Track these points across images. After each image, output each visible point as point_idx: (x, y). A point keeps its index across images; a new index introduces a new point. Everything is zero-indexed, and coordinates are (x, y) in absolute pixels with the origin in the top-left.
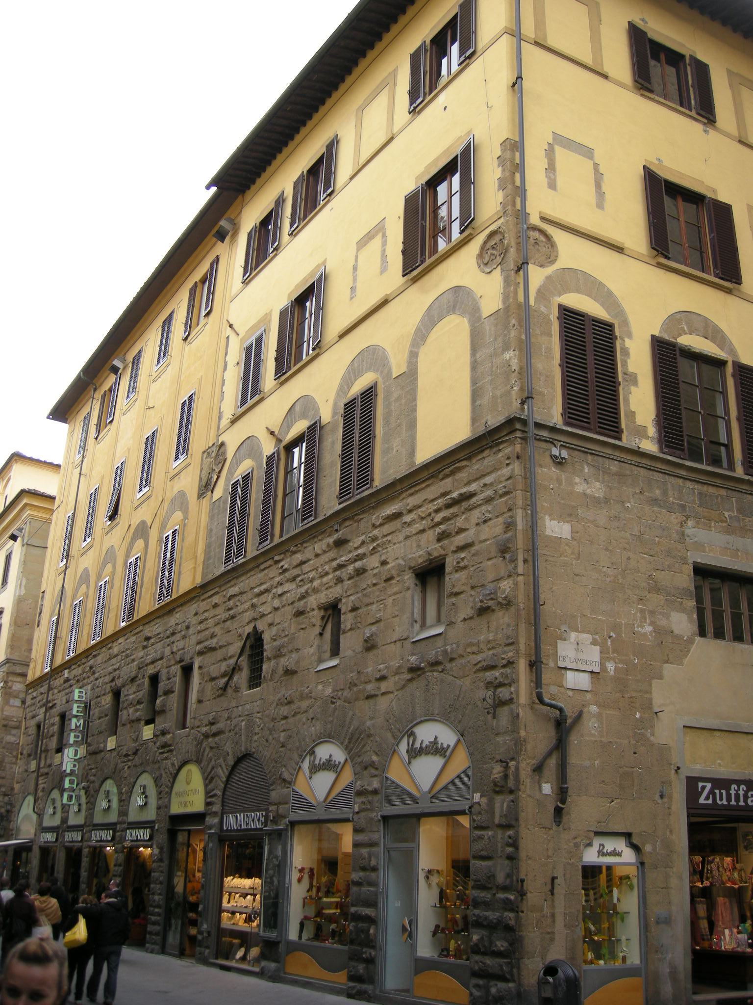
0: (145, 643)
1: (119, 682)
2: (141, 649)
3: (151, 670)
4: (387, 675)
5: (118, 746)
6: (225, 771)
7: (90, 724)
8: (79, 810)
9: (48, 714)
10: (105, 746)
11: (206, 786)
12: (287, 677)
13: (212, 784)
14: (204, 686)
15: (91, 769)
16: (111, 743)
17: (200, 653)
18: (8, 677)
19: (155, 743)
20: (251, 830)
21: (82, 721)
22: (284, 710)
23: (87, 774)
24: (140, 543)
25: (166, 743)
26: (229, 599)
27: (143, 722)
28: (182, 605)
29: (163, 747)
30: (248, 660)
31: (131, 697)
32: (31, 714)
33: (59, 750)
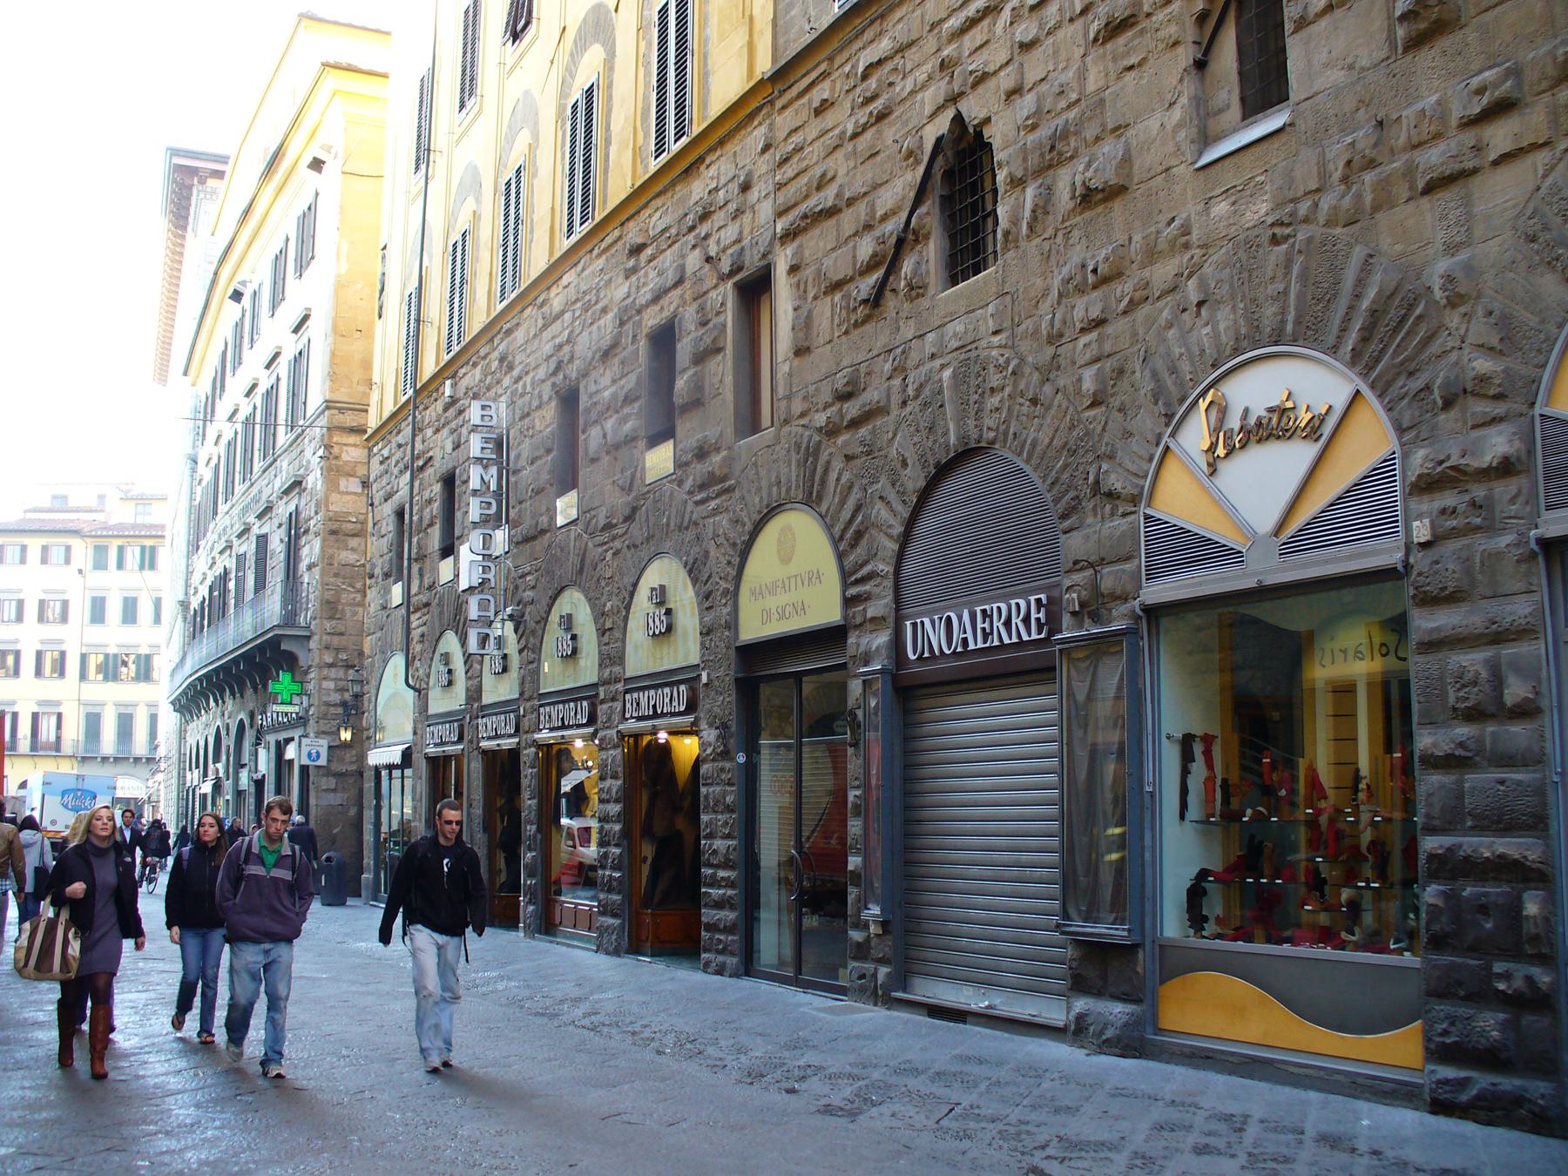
0: (632, 262)
1: (573, 370)
2: (621, 279)
3: (652, 319)
4: (1515, 95)
5: (585, 510)
6: (898, 507)
7: (512, 479)
8: (505, 670)
9: (417, 484)
10: (553, 518)
11: (840, 556)
12: (1088, 215)
13: (859, 550)
14: (810, 312)
15: (523, 576)
16: (566, 508)
17: (789, 235)
18: (331, 437)
19: (680, 483)
20: (1003, 647)
21: (494, 470)
22: (1085, 307)
23: (516, 587)
24: (595, 54)
25: (711, 474)
26: (865, 77)
27: (642, 444)
28: (722, 143)
29: (702, 487)
30: (942, 211)
31: (607, 394)
32: (381, 493)
33: (448, 550)
